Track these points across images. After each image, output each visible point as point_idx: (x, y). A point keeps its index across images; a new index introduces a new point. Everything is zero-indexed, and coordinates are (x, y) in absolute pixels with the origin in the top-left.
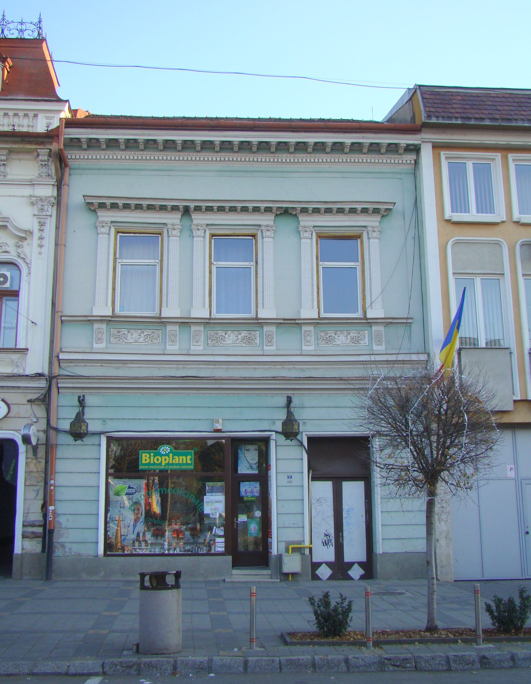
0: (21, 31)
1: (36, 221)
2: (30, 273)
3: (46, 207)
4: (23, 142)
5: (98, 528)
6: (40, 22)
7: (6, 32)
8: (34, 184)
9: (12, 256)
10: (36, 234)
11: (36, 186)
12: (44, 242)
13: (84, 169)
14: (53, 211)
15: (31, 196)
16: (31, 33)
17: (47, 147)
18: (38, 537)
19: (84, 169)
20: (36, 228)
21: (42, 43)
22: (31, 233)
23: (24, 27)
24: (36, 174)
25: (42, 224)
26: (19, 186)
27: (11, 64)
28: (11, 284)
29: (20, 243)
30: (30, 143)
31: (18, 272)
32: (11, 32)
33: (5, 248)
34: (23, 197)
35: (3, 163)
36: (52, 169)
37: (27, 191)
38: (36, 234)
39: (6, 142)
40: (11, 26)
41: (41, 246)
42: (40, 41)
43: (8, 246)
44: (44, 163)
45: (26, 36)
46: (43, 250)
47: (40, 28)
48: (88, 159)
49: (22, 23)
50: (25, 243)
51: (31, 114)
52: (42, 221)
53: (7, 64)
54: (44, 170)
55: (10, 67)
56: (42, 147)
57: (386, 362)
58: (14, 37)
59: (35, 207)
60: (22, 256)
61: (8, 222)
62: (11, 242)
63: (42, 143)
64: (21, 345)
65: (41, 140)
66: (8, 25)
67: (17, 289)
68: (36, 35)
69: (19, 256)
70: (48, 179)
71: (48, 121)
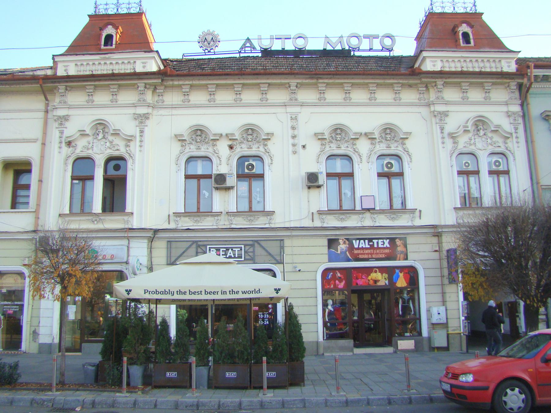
0: (129, 8)
1: (512, 127)
2: (515, 160)
3: (517, 118)
4: (502, 78)
5: (317, 314)
6: (140, 2)
7: (120, 10)
8: (286, 105)
9: (502, 149)
10: (138, 139)
11: (138, 107)
12: (519, 140)
13: (536, 94)
14: (520, 120)
15: (134, 114)
16: (135, 9)
17: (516, 81)
18: (544, 321)
19: (536, 94)
20: (513, 131)
21: (142, 15)
22: (135, 137)
23: (130, 6)
24: (288, 99)
25: (516, 129)
26: (184, 108)
27: (122, 31)
28: (503, 167)
29: (215, 143)
30: (506, 78)
31: (211, 164)
32: (123, 10)
33: (497, 144)
34: (502, 112)
35: (91, 94)
36: (517, 94)
37: (132, 111)
38: (514, 135)
39: (492, 78)
40: (123, 6)
41: (518, 142)
42: (140, 14)
43: (119, 146)
44: (141, 92)
45: (132, 11)
46: (519, 145)
47: (141, 5)
48: (544, 88)
49: (129, 4)
50: (508, 141)
51: (497, 60)
52: (516, 126)
53: (119, 31)
54: (512, 95)
55: (121, 33)
56: (513, 81)
57: (403, 196)
58: (125, 12)
59: (57, 122)
60: (509, 149)
61: (499, 128)
62: (500, 141)
63: (513, 78)
64: (268, 209)
65: (513, 76)
66: (121, 6)
67: (262, 172)
68: (138, 10)
69: (507, 149)
70: (515, 101)
71: (143, 65)
